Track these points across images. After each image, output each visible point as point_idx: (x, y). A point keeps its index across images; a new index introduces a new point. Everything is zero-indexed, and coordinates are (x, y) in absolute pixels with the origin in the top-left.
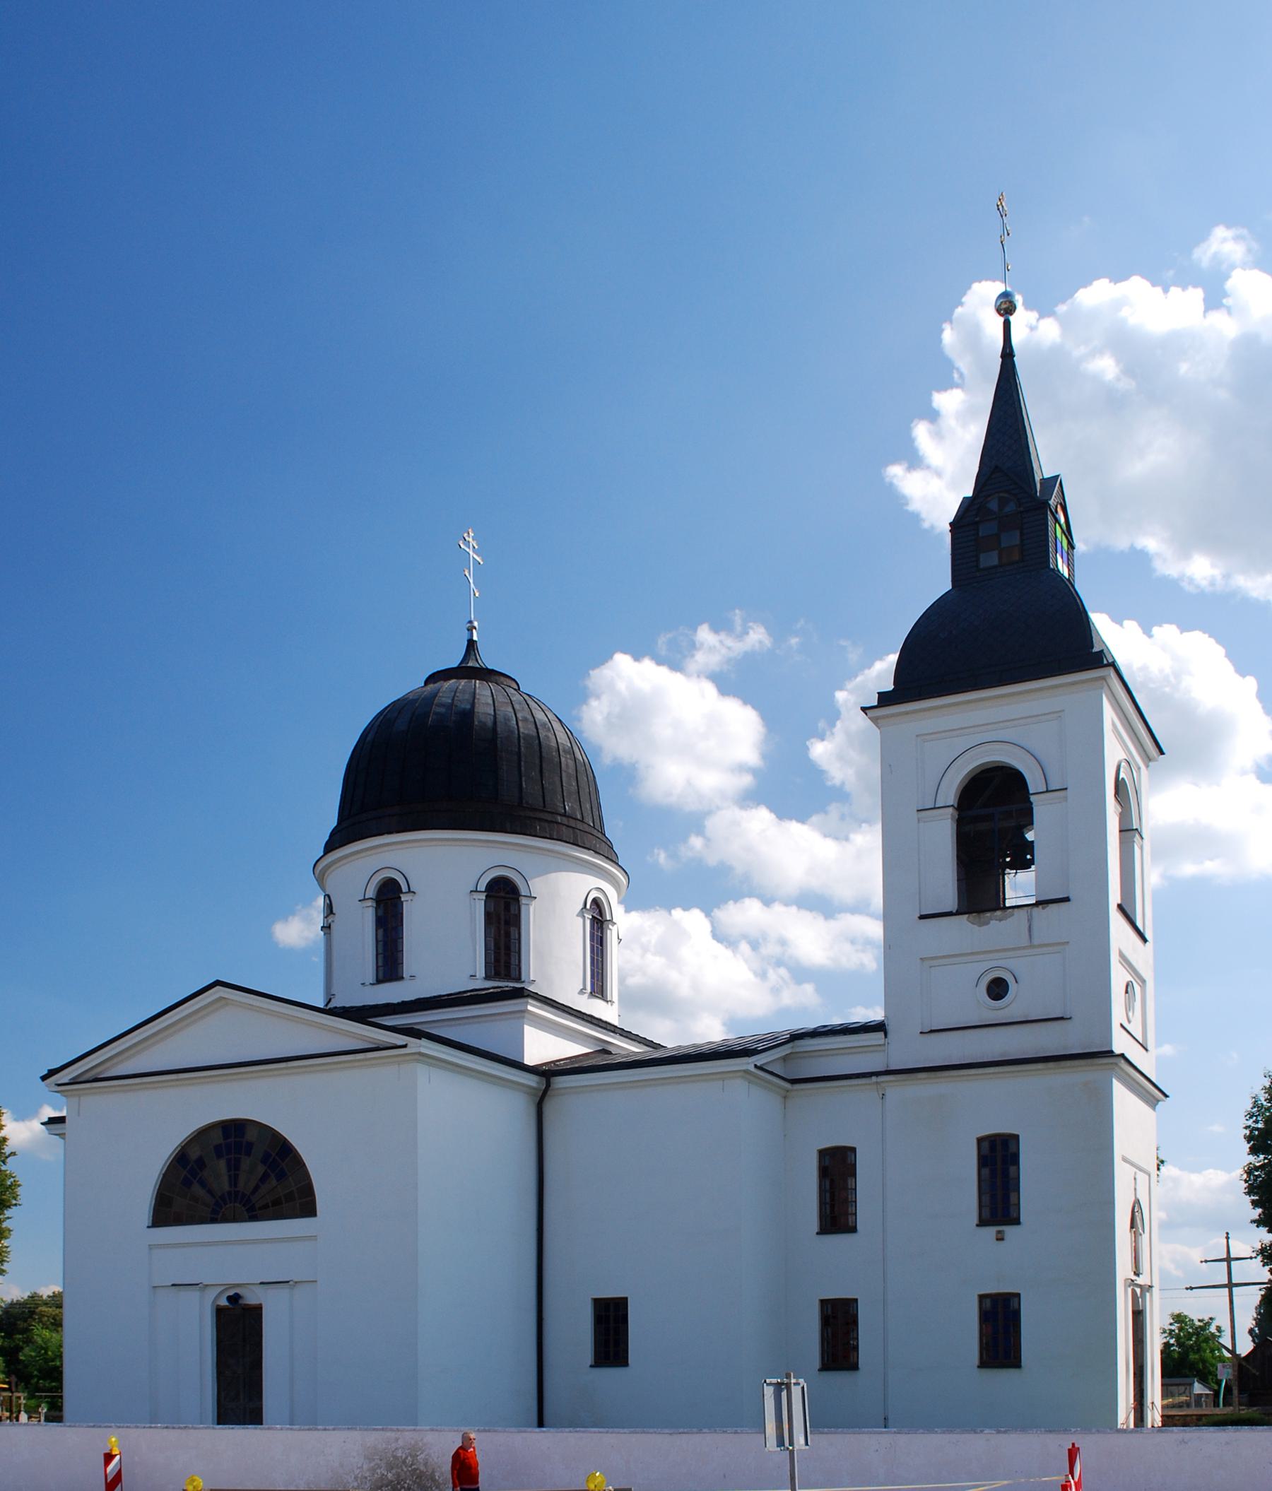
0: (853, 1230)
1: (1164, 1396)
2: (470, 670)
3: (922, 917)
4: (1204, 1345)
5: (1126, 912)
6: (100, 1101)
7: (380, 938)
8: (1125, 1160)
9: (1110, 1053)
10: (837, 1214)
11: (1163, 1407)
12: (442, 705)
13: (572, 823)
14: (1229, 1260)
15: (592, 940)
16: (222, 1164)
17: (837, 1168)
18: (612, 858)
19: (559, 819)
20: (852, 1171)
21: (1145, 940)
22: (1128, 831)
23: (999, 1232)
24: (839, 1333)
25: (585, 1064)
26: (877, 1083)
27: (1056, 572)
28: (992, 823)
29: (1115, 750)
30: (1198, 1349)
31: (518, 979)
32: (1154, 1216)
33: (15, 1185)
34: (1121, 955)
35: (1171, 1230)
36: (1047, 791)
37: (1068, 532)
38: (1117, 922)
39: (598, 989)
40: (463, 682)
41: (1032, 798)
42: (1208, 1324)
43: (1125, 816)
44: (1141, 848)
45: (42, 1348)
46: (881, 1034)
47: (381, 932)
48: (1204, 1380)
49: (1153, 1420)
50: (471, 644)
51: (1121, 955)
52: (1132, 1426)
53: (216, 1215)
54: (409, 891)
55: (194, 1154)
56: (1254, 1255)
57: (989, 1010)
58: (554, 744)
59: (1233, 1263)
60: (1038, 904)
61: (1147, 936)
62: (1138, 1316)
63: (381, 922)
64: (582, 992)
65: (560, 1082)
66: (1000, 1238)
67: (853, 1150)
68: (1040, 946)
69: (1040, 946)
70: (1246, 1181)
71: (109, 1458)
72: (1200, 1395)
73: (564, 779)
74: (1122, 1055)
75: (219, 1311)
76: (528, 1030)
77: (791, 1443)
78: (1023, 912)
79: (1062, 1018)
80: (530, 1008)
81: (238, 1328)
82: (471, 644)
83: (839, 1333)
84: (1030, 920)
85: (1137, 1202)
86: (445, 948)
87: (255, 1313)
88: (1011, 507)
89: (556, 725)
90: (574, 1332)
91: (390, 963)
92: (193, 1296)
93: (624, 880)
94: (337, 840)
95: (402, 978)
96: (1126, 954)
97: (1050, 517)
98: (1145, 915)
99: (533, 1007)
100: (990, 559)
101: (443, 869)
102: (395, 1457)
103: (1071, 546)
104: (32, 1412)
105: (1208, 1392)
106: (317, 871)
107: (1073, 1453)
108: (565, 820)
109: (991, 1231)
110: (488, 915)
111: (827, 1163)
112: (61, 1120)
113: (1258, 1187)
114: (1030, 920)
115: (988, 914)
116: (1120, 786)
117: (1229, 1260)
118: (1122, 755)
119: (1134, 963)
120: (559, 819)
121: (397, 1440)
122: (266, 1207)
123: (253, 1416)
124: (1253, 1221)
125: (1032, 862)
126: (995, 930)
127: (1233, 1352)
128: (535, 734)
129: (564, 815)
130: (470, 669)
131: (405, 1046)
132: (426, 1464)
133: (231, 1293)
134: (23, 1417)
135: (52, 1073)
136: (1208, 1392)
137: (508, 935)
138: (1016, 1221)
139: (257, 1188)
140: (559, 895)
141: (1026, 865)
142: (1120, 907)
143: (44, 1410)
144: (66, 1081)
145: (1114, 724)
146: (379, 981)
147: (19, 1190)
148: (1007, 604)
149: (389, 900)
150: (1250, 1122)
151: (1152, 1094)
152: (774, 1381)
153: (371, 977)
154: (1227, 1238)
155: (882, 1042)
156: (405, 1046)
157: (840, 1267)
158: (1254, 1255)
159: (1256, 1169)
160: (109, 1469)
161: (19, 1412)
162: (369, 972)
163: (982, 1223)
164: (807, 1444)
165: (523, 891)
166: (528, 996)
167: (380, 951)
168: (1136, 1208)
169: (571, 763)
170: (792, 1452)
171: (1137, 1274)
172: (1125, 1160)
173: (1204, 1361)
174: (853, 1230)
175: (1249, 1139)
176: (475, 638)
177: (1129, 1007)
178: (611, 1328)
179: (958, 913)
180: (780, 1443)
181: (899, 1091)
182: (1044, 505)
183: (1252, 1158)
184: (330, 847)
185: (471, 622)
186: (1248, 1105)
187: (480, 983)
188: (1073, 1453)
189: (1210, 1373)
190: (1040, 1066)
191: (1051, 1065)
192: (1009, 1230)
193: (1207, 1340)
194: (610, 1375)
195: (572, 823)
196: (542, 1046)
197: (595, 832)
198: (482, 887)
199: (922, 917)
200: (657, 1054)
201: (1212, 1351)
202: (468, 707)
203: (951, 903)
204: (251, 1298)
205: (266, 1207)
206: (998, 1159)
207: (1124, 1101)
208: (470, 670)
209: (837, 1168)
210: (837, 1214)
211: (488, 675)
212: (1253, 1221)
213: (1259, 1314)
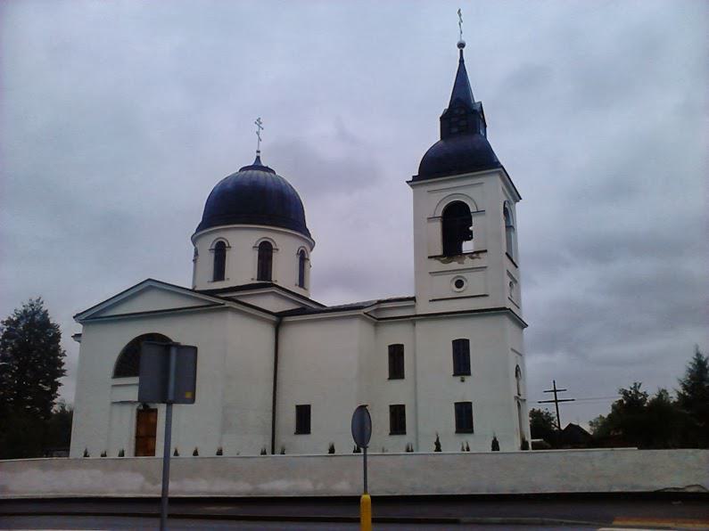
10: (396, 370)
17: (396, 353)
21: (512, 350)
28: (456, 223)
39: (302, 283)
50: (258, 158)
59: (554, 399)
61: (511, 352)
63: (216, 258)
66: (463, 381)
85: (517, 366)
86: (242, 269)
90: (288, 418)
91: (219, 273)
101: (243, 243)
109: (459, 378)
112: (79, 335)
117: (555, 391)
118: (505, 199)
127: (559, 427)
135: (78, 315)
138: (469, 374)
140: (285, 246)
141: (470, 239)
149: (220, 251)
153: (211, 279)
157: (398, 392)
162: (211, 277)
163: (455, 374)
165: (274, 247)
171: (519, 394)
192: (467, 378)
209: (396, 353)
210: (396, 370)
211: (267, 169)
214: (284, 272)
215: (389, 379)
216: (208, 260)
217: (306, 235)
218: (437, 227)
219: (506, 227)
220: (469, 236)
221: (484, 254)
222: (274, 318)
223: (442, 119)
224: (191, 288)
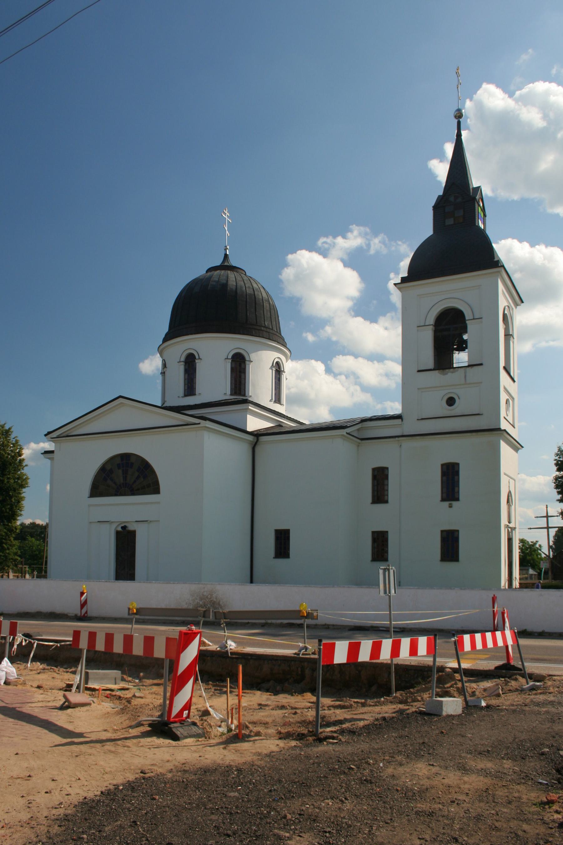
0: (387, 502)
1: (520, 574)
2: (226, 266)
3: (419, 371)
4: (533, 553)
5: (507, 370)
6: (70, 446)
7: (186, 378)
8: (505, 474)
9: (499, 429)
10: (380, 495)
11: (520, 579)
12: (215, 281)
13: (268, 330)
14: (547, 517)
15: (275, 379)
16: (120, 471)
17: (380, 477)
18: (285, 345)
19: (263, 328)
20: (387, 477)
21: (514, 381)
22: (508, 336)
23: (450, 504)
24: (380, 545)
25: (269, 432)
26: (398, 441)
27: (480, 228)
28: (449, 331)
29: (503, 301)
30: (530, 554)
31: (244, 395)
32: (516, 498)
33: (27, 478)
34: (505, 388)
35: (524, 504)
36: (474, 319)
37: (483, 210)
38: (503, 374)
39: (278, 400)
40: (223, 272)
41: (467, 322)
42: (535, 544)
43: (507, 329)
44: (513, 342)
45: (31, 546)
46: (400, 420)
47: (187, 375)
48: (533, 568)
49: (516, 585)
50: (226, 256)
51: (505, 388)
52: (507, 587)
53: (118, 493)
54: (199, 358)
55: (108, 467)
56: (558, 515)
57: (446, 410)
58: (261, 297)
60: (469, 366)
61: (515, 379)
62: (510, 540)
63: (186, 371)
64: (271, 401)
65: (263, 439)
66: (450, 506)
67: (387, 468)
68: (469, 384)
69: (469, 384)
70: (555, 483)
71: (82, 594)
72: (532, 575)
73: (265, 312)
74: (505, 430)
75: (118, 533)
76: (249, 417)
77: (390, 593)
78: (462, 369)
79: (478, 414)
80: (250, 407)
81: (125, 540)
82: (226, 256)
83: (380, 545)
84: (465, 373)
85: (510, 492)
86: (214, 382)
87: (133, 534)
88: (459, 200)
89: (262, 290)
90: (266, 543)
91: (190, 388)
92: (107, 526)
93: (289, 354)
94: (168, 338)
95: (195, 394)
96: (507, 387)
97: (476, 204)
98: (515, 371)
99: (251, 408)
100: (450, 222)
101: (214, 350)
102: (203, 595)
103: (485, 215)
104: (32, 574)
105: (535, 573)
106: (160, 349)
107: (494, 599)
108: (265, 329)
109: (446, 504)
110: (232, 369)
111: (376, 474)
113: (560, 486)
114: (465, 373)
115: (447, 370)
116: (505, 316)
117: (547, 517)
119: (510, 392)
120: (263, 328)
121: (204, 588)
122: (138, 489)
123: (131, 577)
124: (558, 500)
125: (466, 348)
126: (449, 377)
128: (253, 293)
129: (265, 327)
130: (226, 266)
131: (199, 424)
132: (216, 598)
133: (123, 525)
134: (27, 576)
135: (49, 433)
136: (535, 573)
137: (240, 377)
138: (457, 499)
139: (135, 482)
140: (262, 361)
142: (504, 368)
143: (35, 573)
144: (55, 436)
145: (503, 291)
146: (185, 395)
147: (29, 481)
148: (458, 239)
149: (190, 362)
150: (557, 458)
151: (516, 446)
152: (383, 567)
154: (547, 507)
155: (400, 423)
156: (199, 424)
157: (381, 518)
158: (558, 515)
159: (560, 478)
160: (82, 598)
161: (25, 574)
163: (443, 500)
164: (395, 593)
165: (247, 359)
166: (249, 403)
167: (186, 383)
168: (509, 494)
169: (268, 305)
170: (390, 597)
171: (509, 522)
172: (505, 474)
173: (533, 560)
174: (387, 502)
175: (556, 464)
176: (228, 253)
177: (507, 409)
178: (282, 542)
179: (434, 370)
180: (385, 592)
181: (407, 444)
182: (474, 199)
183: (558, 473)
184: (165, 340)
185: (226, 246)
186: (556, 451)
187: (228, 397)
188: (494, 599)
189: (536, 565)
190: (469, 434)
191: (474, 434)
192: (454, 503)
193: (535, 550)
194: (282, 562)
195: (268, 330)
196: (254, 423)
197: (277, 334)
198: (230, 357)
199: (419, 371)
200: (303, 427)
201: (537, 555)
202: (225, 282)
203: (431, 365)
204: (131, 528)
205: (138, 489)
206: (450, 474)
207: (505, 449)
208: (226, 266)
209: (380, 477)
210: (380, 495)
212: (558, 500)
213: (555, 539)
214: (260, 386)
215: (371, 503)
216: (178, 373)
217: (279, 343)
218: (428, 336)
219: (505, 335)
220: (462, 346)
221: (481, 366)
222: (251, 438)
223: (435, 208)
224: (160, 405)
